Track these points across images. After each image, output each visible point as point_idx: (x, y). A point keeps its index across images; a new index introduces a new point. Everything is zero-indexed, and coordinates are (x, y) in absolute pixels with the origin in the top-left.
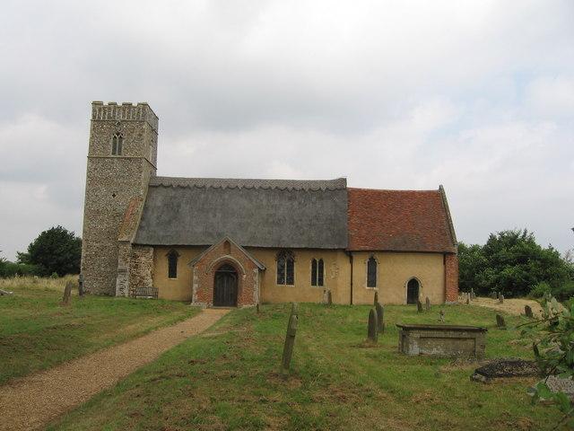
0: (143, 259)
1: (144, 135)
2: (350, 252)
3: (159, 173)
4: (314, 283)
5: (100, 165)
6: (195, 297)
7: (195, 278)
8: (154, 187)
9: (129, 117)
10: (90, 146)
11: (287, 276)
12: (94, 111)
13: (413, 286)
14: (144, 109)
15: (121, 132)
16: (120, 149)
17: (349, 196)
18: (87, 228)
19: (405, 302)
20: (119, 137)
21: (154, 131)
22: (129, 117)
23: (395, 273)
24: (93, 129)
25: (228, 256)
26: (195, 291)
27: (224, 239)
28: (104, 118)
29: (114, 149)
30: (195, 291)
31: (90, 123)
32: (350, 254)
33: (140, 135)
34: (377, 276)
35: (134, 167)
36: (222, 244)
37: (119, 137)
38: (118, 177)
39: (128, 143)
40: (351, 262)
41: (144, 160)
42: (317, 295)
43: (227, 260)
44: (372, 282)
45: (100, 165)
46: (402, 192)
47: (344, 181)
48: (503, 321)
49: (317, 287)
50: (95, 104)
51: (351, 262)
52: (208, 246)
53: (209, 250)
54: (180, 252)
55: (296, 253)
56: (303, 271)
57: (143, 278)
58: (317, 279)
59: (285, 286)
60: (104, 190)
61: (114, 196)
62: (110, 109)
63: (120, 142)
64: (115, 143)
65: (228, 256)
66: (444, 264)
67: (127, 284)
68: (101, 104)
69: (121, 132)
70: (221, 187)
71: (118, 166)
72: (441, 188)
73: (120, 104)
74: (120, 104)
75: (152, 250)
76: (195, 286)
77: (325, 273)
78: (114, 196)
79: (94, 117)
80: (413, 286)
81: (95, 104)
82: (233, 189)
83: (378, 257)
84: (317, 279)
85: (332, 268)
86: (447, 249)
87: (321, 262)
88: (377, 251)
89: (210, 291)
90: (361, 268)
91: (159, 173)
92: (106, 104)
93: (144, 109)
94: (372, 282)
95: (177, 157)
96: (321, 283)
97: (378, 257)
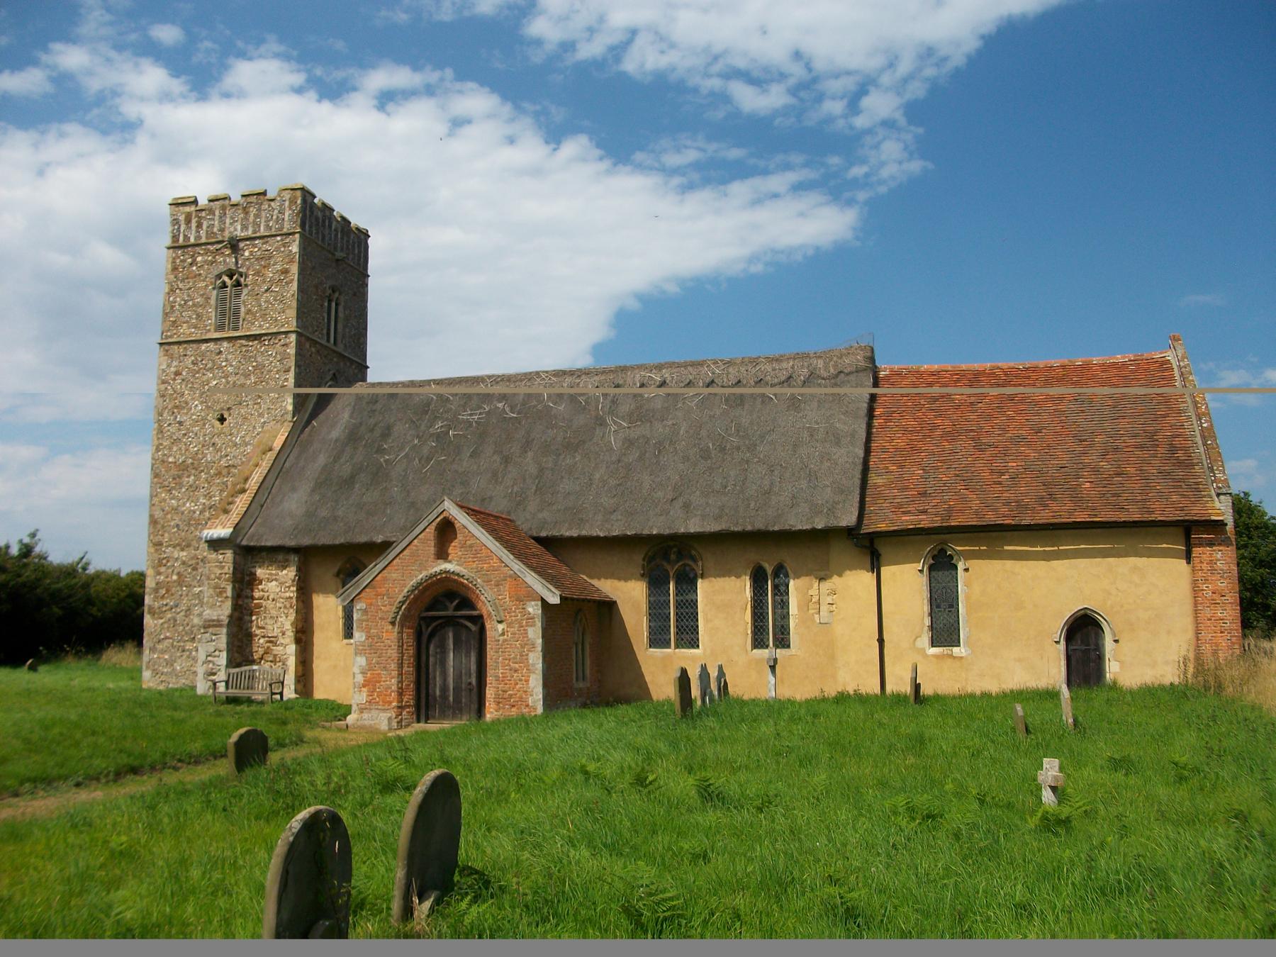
2: (874, 537)
4: (759, 641)
12: (175, 222)
13: (1083, 632)
44: (944, 630)
56: (723, 600)
57: (273, 641)
58: (769, 629)
60: (197, 407)
61: (222, 420)
62: (211, 212)
78: (222, 420)
79: (175, 238)
80: (1083, 632)
84: (769, 629)
86: (1195, 512)
90: (906, 581)
94: (944, 630)
96: (783, 641)
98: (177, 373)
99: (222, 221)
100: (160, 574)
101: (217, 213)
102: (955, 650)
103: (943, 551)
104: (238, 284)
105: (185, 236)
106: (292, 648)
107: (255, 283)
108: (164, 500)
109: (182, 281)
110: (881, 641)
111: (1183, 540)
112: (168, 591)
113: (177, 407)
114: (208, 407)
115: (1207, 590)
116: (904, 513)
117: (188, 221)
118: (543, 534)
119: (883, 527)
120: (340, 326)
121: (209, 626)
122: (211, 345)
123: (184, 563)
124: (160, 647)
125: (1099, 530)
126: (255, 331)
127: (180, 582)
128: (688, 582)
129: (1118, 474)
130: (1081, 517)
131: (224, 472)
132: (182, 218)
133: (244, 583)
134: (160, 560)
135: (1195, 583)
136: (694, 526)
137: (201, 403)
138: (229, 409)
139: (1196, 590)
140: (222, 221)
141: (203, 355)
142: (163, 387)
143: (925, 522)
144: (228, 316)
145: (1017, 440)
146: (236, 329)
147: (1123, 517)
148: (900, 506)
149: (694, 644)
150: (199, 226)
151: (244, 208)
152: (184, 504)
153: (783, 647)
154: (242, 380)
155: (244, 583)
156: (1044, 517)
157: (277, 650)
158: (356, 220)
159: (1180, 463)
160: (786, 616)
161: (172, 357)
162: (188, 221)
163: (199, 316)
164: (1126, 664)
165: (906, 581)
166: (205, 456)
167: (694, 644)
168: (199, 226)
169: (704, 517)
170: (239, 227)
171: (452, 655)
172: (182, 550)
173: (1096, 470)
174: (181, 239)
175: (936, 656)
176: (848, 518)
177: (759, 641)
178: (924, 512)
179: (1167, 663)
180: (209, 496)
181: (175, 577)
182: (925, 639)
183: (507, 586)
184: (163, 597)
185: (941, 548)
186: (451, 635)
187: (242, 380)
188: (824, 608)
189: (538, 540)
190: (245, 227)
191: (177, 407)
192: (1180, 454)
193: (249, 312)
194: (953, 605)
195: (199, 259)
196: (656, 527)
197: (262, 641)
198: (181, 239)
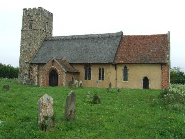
0: (34, 69)
2: (116, 64)
4: (100, 79)
6: (41, 85)
8: (45, 41)
10: (22, 26)
11: (88, 76)
12: (24, 12)
13: (146, 81)
14: (40, 10)
15: (36, 21)
16: (32, 26)
18: (21, 58)
19: (142, 88)
23: (137, 74)
24: (23, 19)
29: (30, 26)
31: (22, 17)
32: (115, 65)
33: (38, 20)
35: (36, 33)
40: (116, 69)
41: (39, 30)
42: (103, 85)
43: (56, 70)
44: (126, 79)
46: (148, 36)
47: (122, 33)
48: (41, 126)
49: (101, 81)
51: (116, 69)
55: (92, 65)
56: (95, 72)
58: (101, 77)
59: (88, 80)
61: (30, 45)
62: (28, 11)
63: (32, 23)
66: (162, 70)
69: (36, 21)
75: (37, 66)
77: (104, 75)
79: (23, 15)
80: (146, 81)
81: (24, 10)
82: (74, 39)
83: (128, 67)
84: (101, 77)
86: (163, 62)
87: (103, 69)
88: (127, 64)
89: (47, 82)
90: (120, 71)
92: (32, 9)
93: (40, 10)
94: (126, 79)
96: (103, 79)
97: (128, 67)
98: (24, 35)
99: (30, 12)
110: (116, 80)
111: (161, 66)
115: (164, 74)
117: (25, 12)
118: (70, 62)
119: (117, 63)
120: (48, 28)
122: (28, 31)
124: (20, 77)
126: (34, 29)
127: (23, 68)
133: (30, 68)
135: (162, 73)
136: (91, 62)
139: (162, 74)
140: (30, 12)
143: (123, 62)
144: (31, 27)
145: (140, 50)
146: (32, 28)
149: (91, 79)
150: (27, 13)
155: (30, 68)
157: (35, 78)
158: (50, 12)
159: (163, 55)
161: (23, 32)
162: (25, 12)
164: (151, 85)
165: (120, 71)
167: (91, 79)
168: (27, 13)
173: (150, 55)
176: (111, 62)
177: (100, 79)
180: (27, 56)
183: (60, 70)
185: (126, 66)
188: (108, 75)
189: (69, 63)
190: (33, 13)
193: (34, 26)
194: (127, 75)
196: (85, 62)
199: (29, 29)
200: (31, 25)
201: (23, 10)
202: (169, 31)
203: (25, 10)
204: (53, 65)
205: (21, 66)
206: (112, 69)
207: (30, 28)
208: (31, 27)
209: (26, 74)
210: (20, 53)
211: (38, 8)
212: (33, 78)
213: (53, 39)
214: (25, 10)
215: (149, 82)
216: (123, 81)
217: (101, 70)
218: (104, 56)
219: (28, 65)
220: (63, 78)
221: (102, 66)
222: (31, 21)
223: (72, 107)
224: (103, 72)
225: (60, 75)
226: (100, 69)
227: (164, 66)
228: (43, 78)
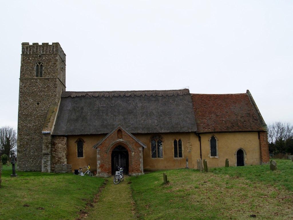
0: (60, 145)
1: (57, 63)
3: (68, 89)
4: (176, 156)
5: (28, 84)
6: (99, 170)
7: (98, 156)
9: (46, 52)
12: (23, 48)
13: (240, 154)
15: (42, 63)
16: (41, 73)
17: (192, 99)
19: (236, 165)
20: (39, 67)
21: (63, 61)
22: (46, 52)
25: (121, 140)
26: (98, 166)
27: (116, 129)
28: (30, 53)
29: (37, 73)
30: (98, 166)
32: (198, 135)
33: (55, 64)
34: (217, 148)
36: (116, 131)
37: (39, 67)
38: (41, 91)
39: (47, 69)
40: (200, 140)
41: (57, 80)
43: (120, 143)
44: (214, 153)
45: (28, 84)
47: (188, 90)
49: (179, 158)
50: (23, 44)
51: (200, 140)
52: (107, 134)
53: (108, 136)
54: (85, 139)
56: (167, 146)
57: (60, 158)
61: (38, 104)
63: (41, 68)
64: (37, 69)
65: (121, 140)
66: (259, 138)
67: (49, 163)
68: (28, 44)
69: (42, 63)
70: (120, 95)
71: (40, 84)
72: (248, 91)
73: (40, 44)
74: (40, 44)
76: (99, 162)
77: (183, 149)
78: (38, 104)
79: (23, 52)
80: (240, 154)
81: (23, 44)
83: (217, 136)
85: (188, 145)
86: (260, 129)
87: (180, 141)
88: (215, 132)
91: (30, 44)
92: (31, 44)
94: (214, 153)
95: (79, 78)
97: (217, 136)
98: (25, 87)
100: (21, 142)
101: (35, 47)
102: (216, 157)
103: (213, 137)
104: (41, 65)
105: (26, 52)
106: (66, 160)
107: (46, 66)
108: (22, 123)
109: (26, 64)
112: (23, 147)
113: (25, 100)
114: (34, 101)
116: (205, 129)
121: (45, 155)
123: (28, 139)
125: (254, 132)
128: (160, 142)
129: (245, 122)
130: (240, 130)
131: (39, 117)
132: (25, 48)
133: (53, 144)
134: (21, 139)
136: (163, 131)
137: (32, 99)
138: (40, 101)
141: (32, 82)
142: (21, 90)
143: (210, 130)
144: (39, 73)
147: (248, 130)
148: (204, 127)
150: (30, 50)
151: (43, 47)
152: (28, 125)
153: (180, 157)
154: (44, 89)
156: (233, 130)
157: (62, 160)
160: (181, 150)
161: (23, 82)
163: (31, 73)
166: (33, 113)
168: (30, 50)
169: (165, 129)
170: (42, 51)
171: (120, 160)
172: (27, 136)
173: (240, 121)
174: (25, 53)
175: (212, 158)
177: (176, 156)
178: (209, 129)
179: (255, 158)
180: (35, 122)
181: (25, 143)
182: (210, 155)
184: (22, 148)
186: (120, 155)
187: (44, 89)
190: (43, 52)
191: (25, 100)
192: (255, 118)
193: (45, 73)
195: (30, 58)
197: (57, 158)
198: (25, 53)
199: (37, 78)
200: (39, 70)
201: (21, 45)
202: (248, 91)
203: (25, 46)
204: (118, 138)
205: (21, 139)
206: (194, 141)
207: (37, 76)
208: (39, 73)
209: (47, 154)
210: (19, 117)
211: (53, 43)
212: (58, 161)
213: (67, 96)
214: (25, 46)
215: (245, 155)
216: (211, 157)
217: (178, 142)
218: (187, 123)
219: (50, 138)
220: (136, 156)
221: (178, 135)
222: (40, 63)
223: (258, 188)
224: (180, 145)
225: (133, 153)
226: (175, 142)
227: (262, 134)
228: (102, 159)
